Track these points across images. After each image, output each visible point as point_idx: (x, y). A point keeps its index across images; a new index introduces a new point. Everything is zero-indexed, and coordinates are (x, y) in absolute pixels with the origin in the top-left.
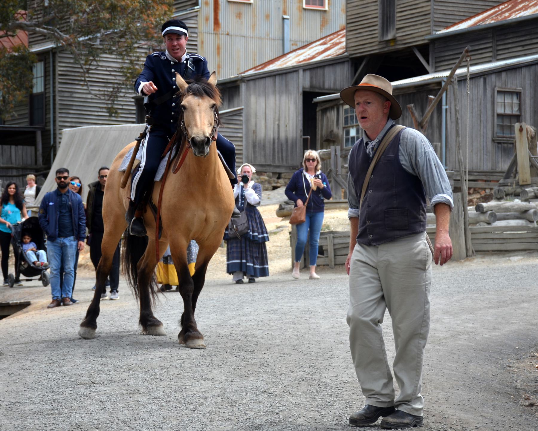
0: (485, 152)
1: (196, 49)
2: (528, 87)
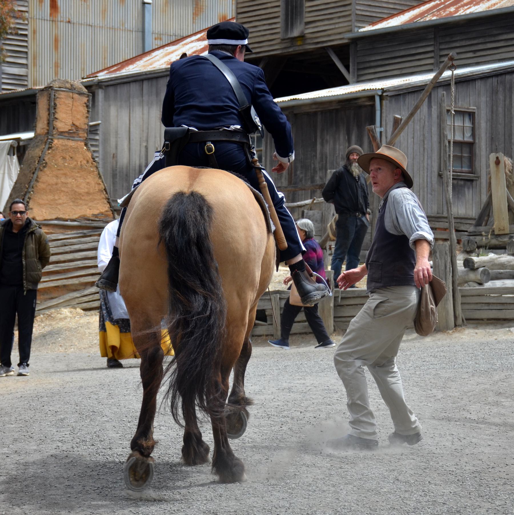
0: (429, 191)
1: (26, 41)
2: (483, 106)
